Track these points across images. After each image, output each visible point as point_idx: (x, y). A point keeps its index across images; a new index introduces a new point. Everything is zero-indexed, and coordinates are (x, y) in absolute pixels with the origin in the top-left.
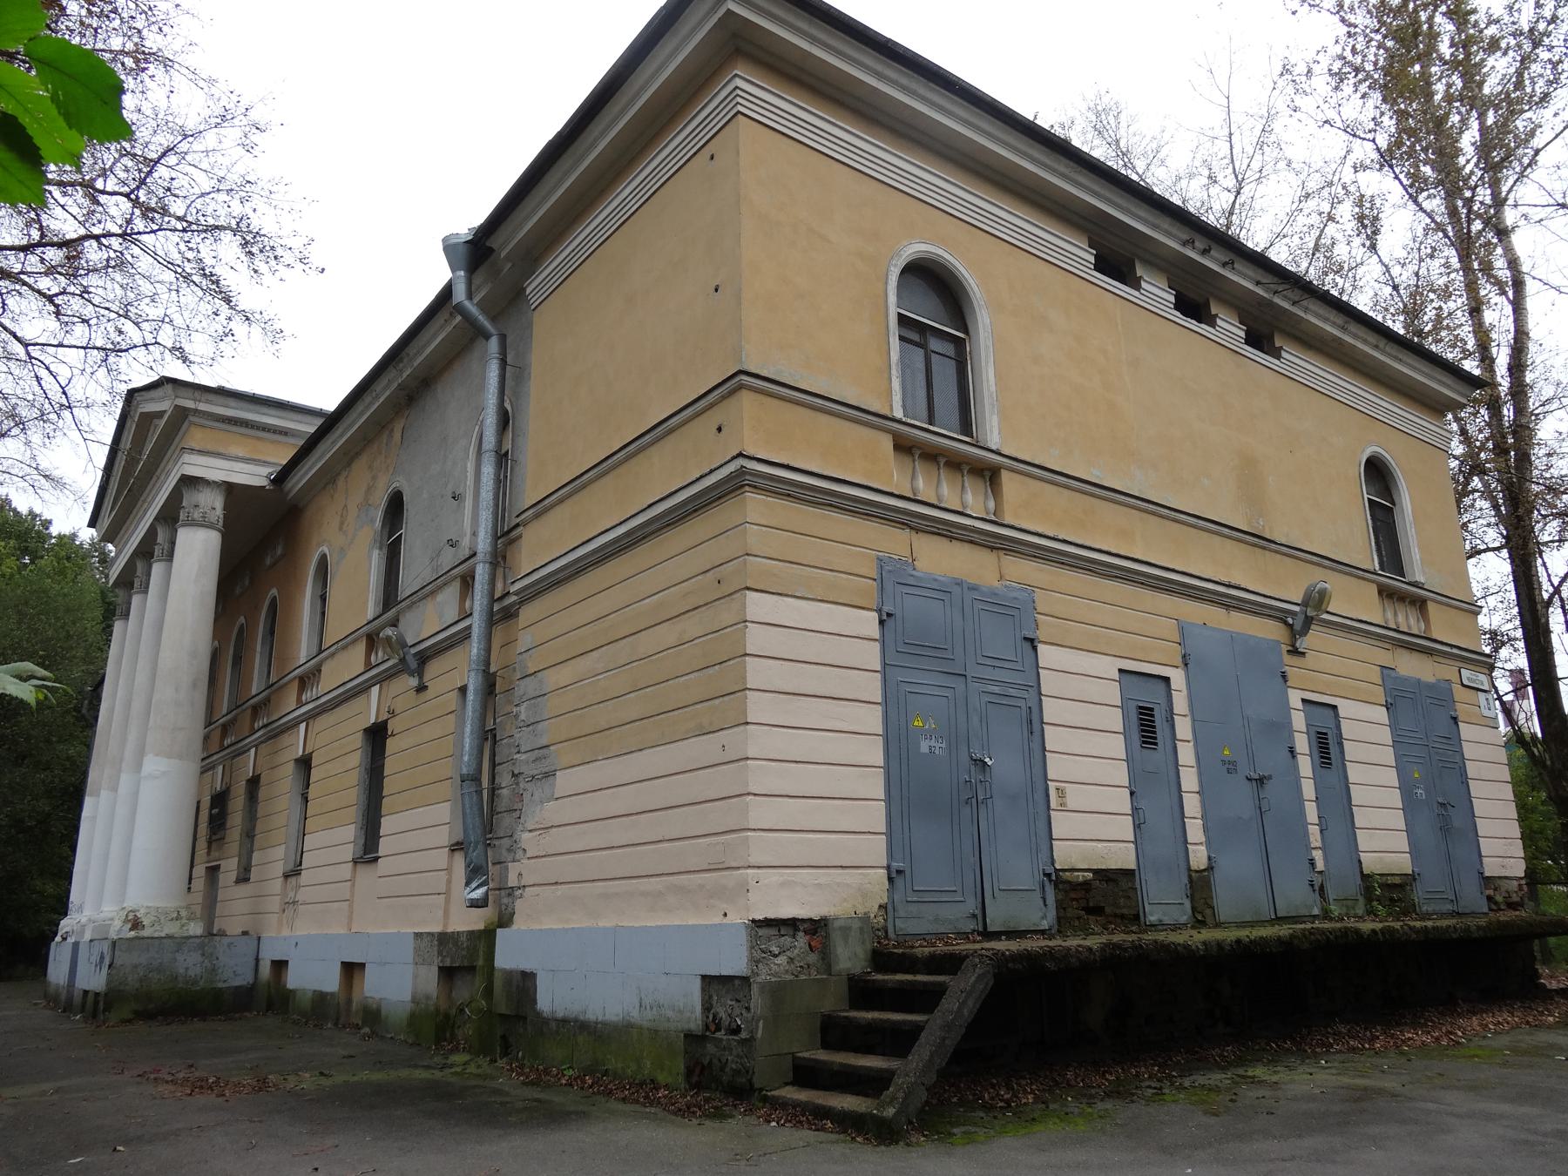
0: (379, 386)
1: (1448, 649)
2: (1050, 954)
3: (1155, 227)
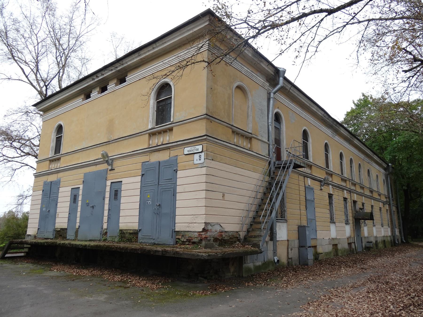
0: (310, 102)
1: (176, 144)
2: (53, 243)
3: (88, 82)
